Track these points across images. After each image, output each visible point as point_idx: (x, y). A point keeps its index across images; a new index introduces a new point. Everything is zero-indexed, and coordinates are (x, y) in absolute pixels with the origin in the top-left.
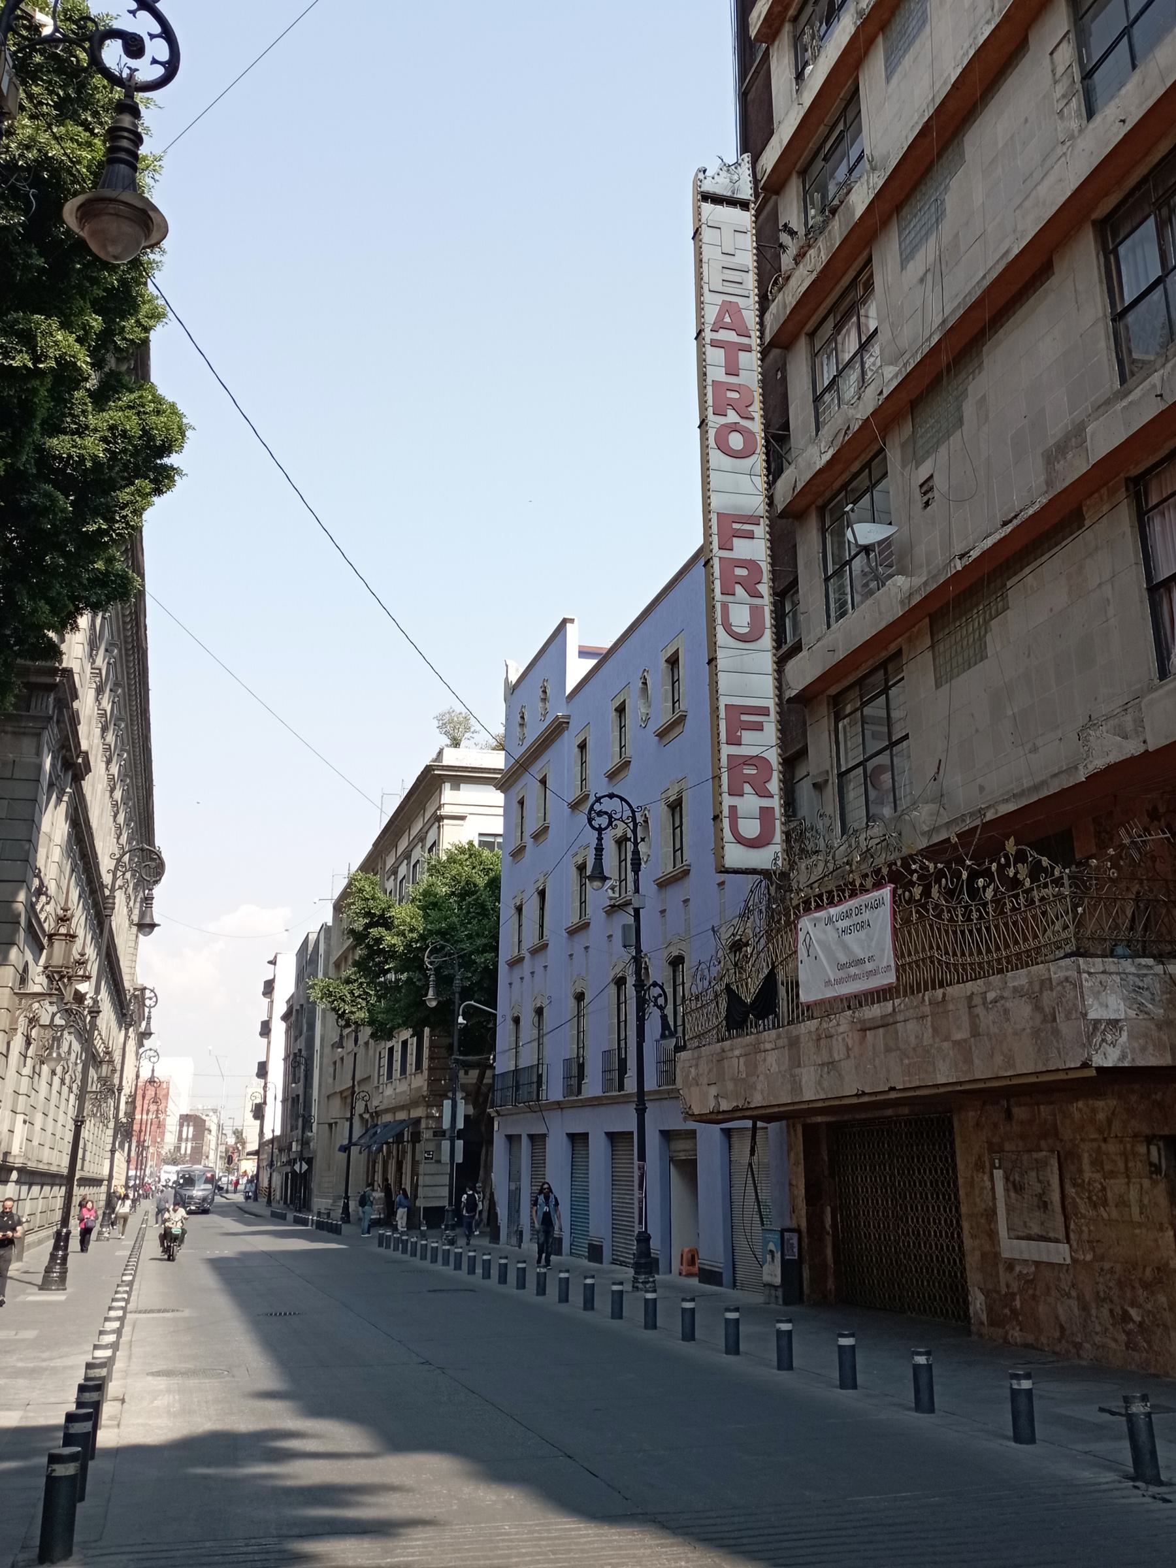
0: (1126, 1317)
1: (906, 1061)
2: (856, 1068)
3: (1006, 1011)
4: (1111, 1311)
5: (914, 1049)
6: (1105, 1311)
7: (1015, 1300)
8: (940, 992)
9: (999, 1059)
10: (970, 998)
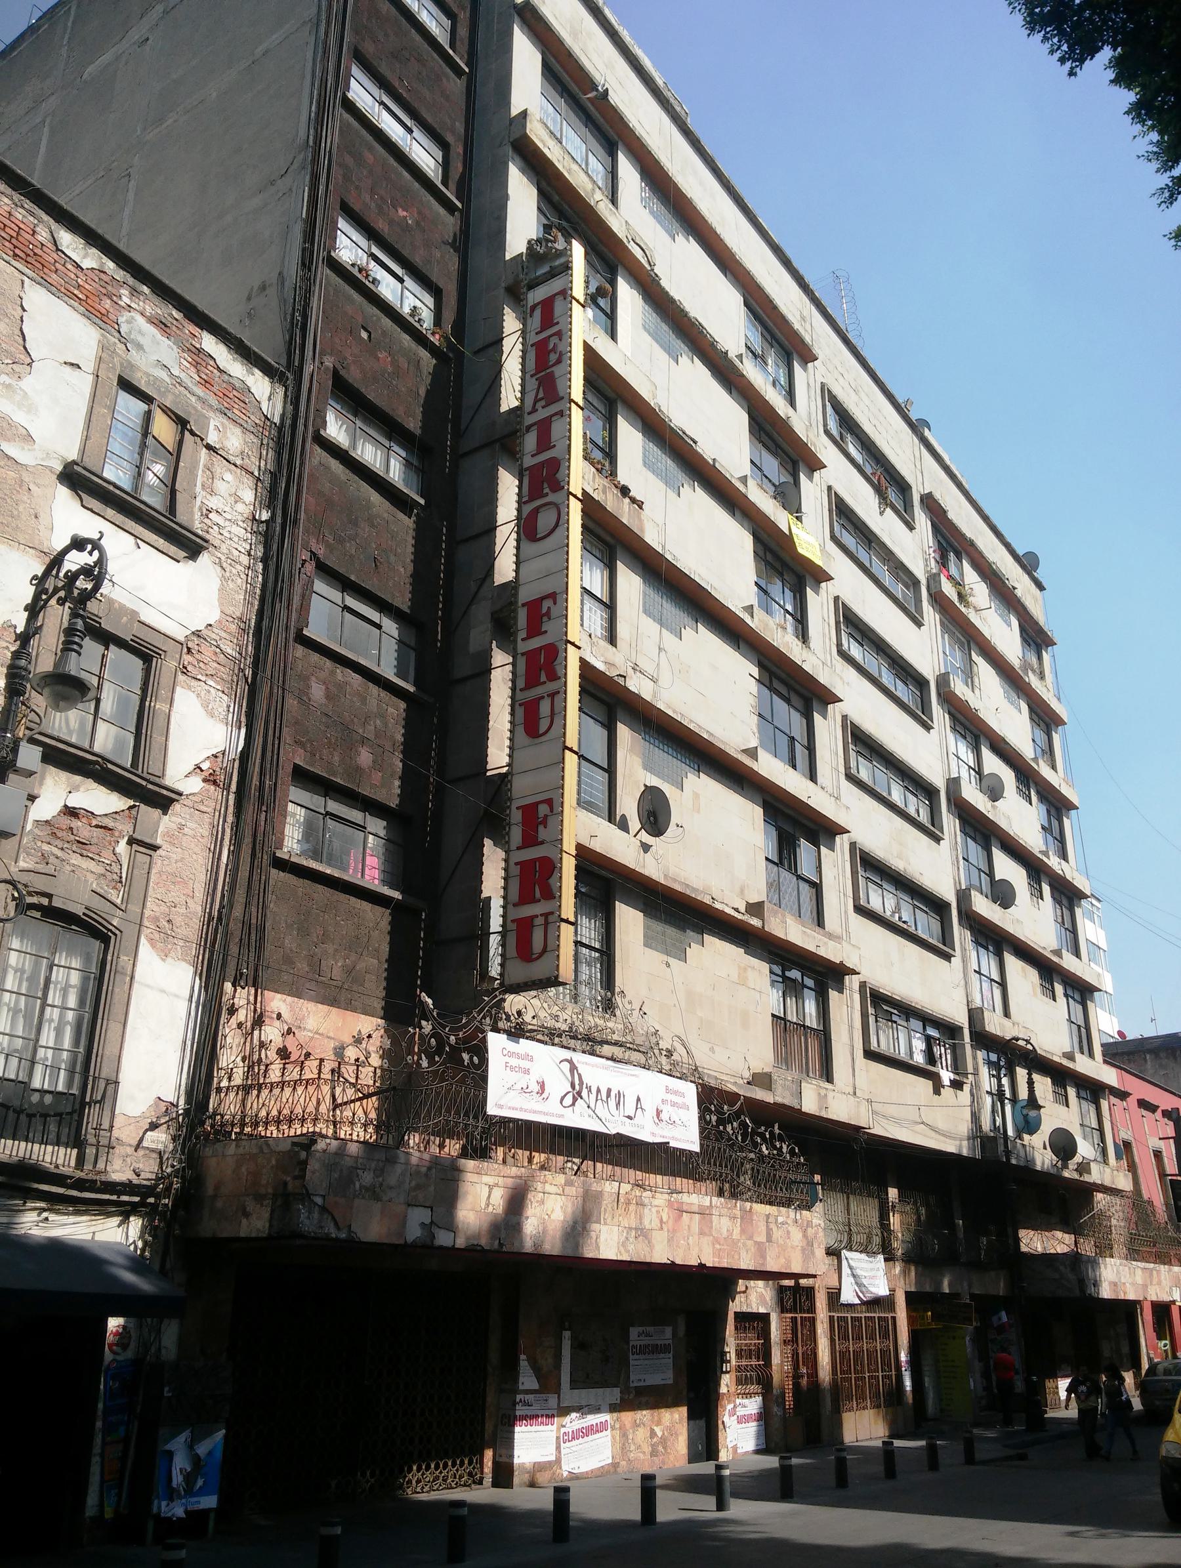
1: (718, 1246)
3: (788, 1232)
10: (768, 1216)
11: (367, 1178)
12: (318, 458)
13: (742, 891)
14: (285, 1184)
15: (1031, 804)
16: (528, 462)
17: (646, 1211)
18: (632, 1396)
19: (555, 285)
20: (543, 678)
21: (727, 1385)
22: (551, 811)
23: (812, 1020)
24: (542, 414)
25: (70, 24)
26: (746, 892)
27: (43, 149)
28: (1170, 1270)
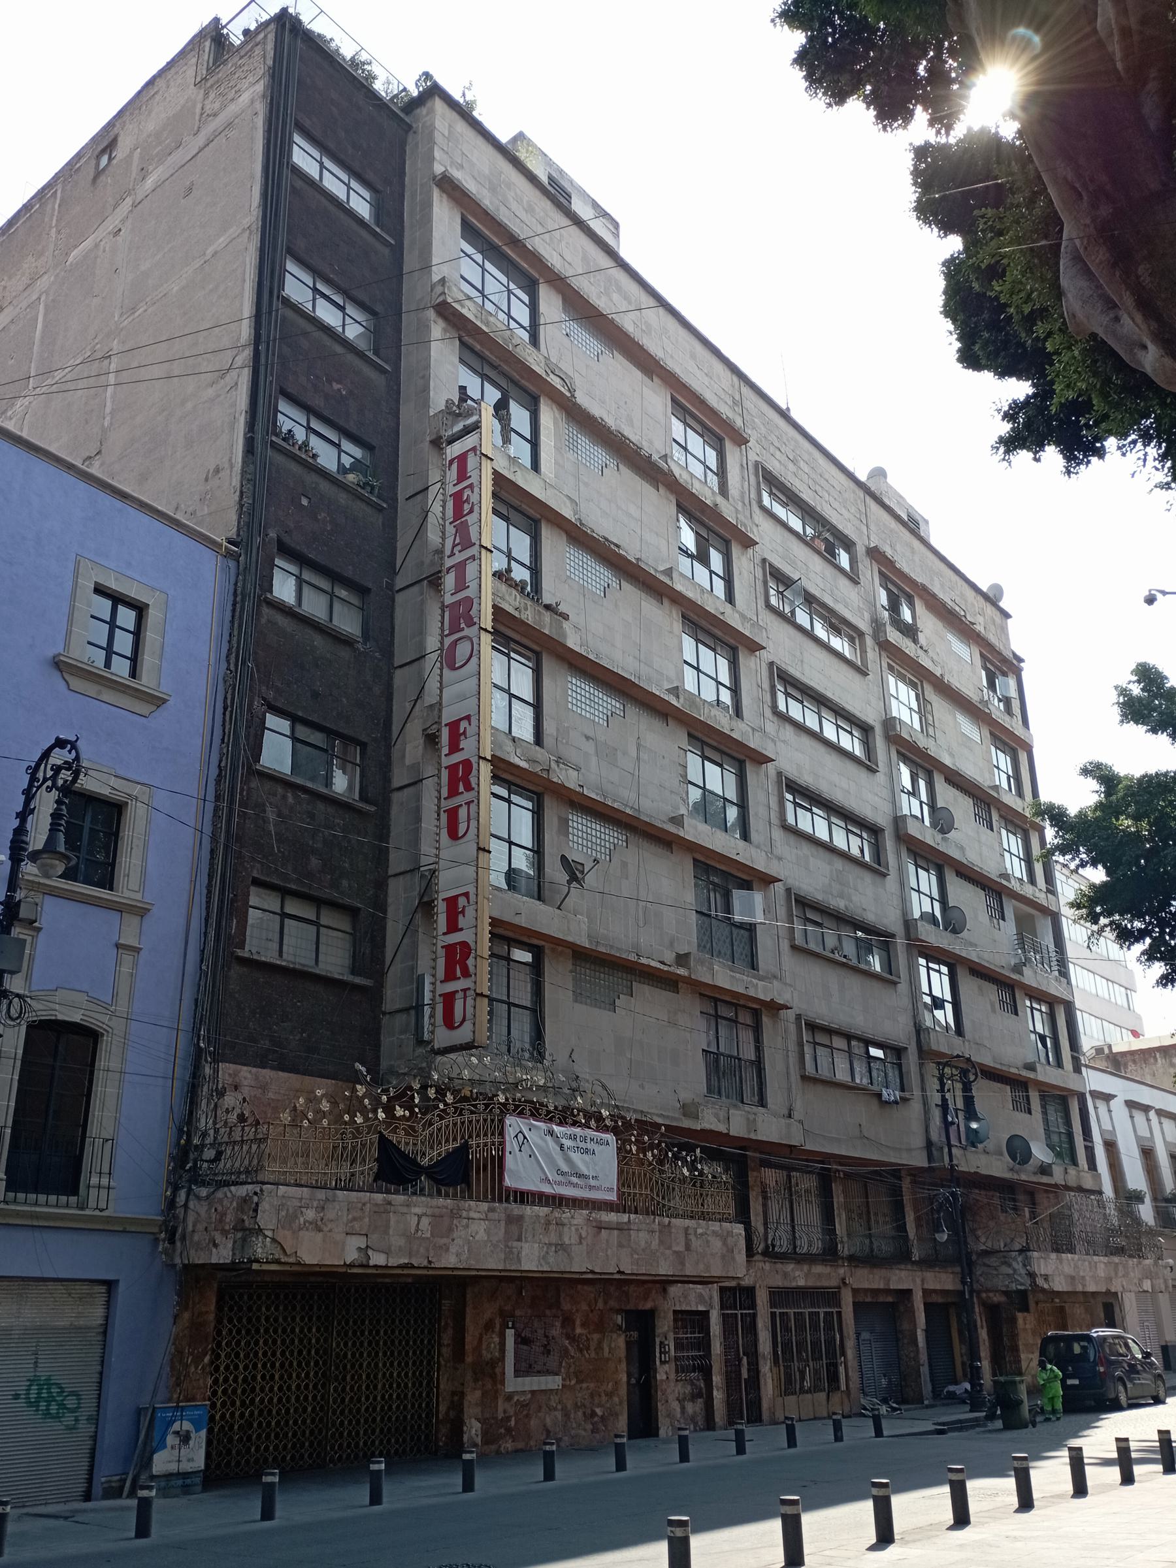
0: (594, 1414)
1: (636, 1256)
2: (588, 1253)
3: (708, 1242)
4: (584, 1413)
5: (643, 1250)
6: (580, 1414)
7: (510, 1421)
8: (667, 1220)
9: (701, 1266)
10: (687, 1229)
11: (310, 1214)
12: (266, 617)
13: (672, 944)
14: (243, 1221)
15: (992, 830)
16: (449, 599)
17: (566, 1229)
18: (573, 1382)
19: (469, 441)
20: (461, 789)
21: (666, 1373)
22: (468, 902)
23: (749, 1053)
24: (459, 557)
25: (57, 207)
26: (676, 944)
27: (40, 326)
28: (1140, 1263)
